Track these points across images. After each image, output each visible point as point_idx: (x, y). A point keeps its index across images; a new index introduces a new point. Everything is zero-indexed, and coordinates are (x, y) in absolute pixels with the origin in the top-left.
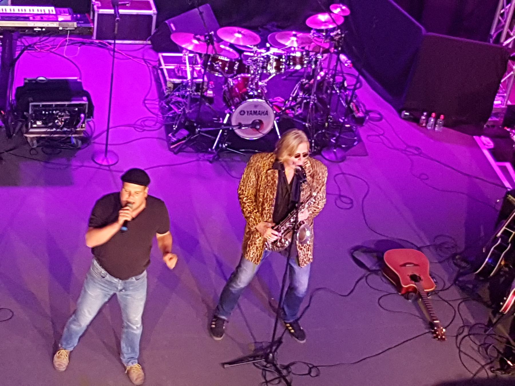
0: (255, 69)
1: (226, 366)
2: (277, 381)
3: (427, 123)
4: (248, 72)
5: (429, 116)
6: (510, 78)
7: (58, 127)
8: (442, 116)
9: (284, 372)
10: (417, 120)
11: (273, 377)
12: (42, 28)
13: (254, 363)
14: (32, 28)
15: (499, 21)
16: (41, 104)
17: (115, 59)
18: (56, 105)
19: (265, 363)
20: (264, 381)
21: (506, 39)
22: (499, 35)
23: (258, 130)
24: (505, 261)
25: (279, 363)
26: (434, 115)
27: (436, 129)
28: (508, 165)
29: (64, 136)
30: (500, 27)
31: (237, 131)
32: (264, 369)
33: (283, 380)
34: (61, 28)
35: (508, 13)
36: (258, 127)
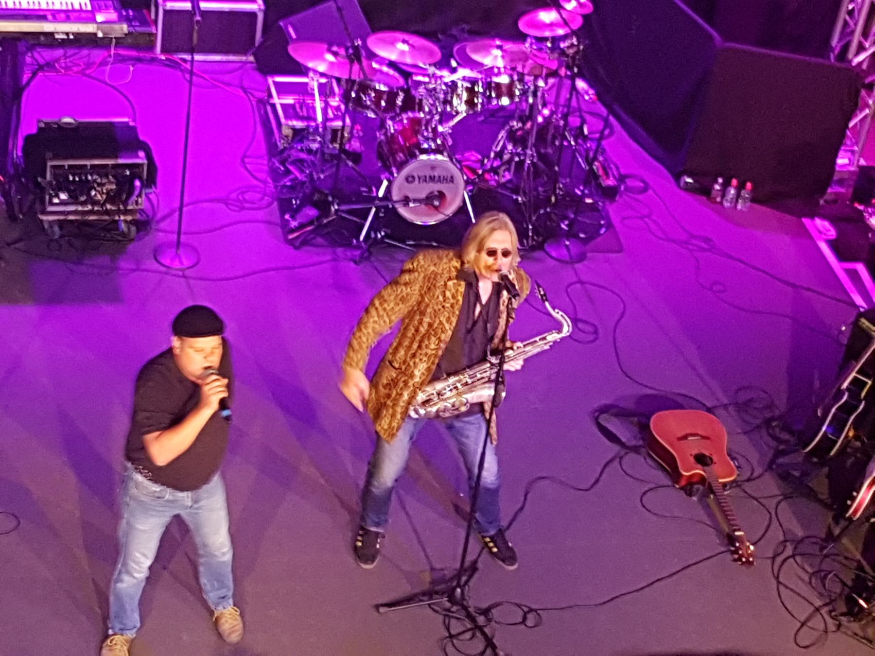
1: (382, 610)
2: (468, 635)
4: (421, 109)
5: (726, 185)
7: (94, 203)
9: (481, 620)
11: (461, 629)
12: (67, 34)
14: (52, 34)
15: (846, 23)
19: (448, 605)
22: (845, 48)
23: (436, 208)
24: (855, 429)
25: (472, 604)
26: (734, 182)
27: (739, 207)
28: (861, 268)
30: (848, 32)
31: (402, 211)
32: (447, 614)
35: (860, 11)
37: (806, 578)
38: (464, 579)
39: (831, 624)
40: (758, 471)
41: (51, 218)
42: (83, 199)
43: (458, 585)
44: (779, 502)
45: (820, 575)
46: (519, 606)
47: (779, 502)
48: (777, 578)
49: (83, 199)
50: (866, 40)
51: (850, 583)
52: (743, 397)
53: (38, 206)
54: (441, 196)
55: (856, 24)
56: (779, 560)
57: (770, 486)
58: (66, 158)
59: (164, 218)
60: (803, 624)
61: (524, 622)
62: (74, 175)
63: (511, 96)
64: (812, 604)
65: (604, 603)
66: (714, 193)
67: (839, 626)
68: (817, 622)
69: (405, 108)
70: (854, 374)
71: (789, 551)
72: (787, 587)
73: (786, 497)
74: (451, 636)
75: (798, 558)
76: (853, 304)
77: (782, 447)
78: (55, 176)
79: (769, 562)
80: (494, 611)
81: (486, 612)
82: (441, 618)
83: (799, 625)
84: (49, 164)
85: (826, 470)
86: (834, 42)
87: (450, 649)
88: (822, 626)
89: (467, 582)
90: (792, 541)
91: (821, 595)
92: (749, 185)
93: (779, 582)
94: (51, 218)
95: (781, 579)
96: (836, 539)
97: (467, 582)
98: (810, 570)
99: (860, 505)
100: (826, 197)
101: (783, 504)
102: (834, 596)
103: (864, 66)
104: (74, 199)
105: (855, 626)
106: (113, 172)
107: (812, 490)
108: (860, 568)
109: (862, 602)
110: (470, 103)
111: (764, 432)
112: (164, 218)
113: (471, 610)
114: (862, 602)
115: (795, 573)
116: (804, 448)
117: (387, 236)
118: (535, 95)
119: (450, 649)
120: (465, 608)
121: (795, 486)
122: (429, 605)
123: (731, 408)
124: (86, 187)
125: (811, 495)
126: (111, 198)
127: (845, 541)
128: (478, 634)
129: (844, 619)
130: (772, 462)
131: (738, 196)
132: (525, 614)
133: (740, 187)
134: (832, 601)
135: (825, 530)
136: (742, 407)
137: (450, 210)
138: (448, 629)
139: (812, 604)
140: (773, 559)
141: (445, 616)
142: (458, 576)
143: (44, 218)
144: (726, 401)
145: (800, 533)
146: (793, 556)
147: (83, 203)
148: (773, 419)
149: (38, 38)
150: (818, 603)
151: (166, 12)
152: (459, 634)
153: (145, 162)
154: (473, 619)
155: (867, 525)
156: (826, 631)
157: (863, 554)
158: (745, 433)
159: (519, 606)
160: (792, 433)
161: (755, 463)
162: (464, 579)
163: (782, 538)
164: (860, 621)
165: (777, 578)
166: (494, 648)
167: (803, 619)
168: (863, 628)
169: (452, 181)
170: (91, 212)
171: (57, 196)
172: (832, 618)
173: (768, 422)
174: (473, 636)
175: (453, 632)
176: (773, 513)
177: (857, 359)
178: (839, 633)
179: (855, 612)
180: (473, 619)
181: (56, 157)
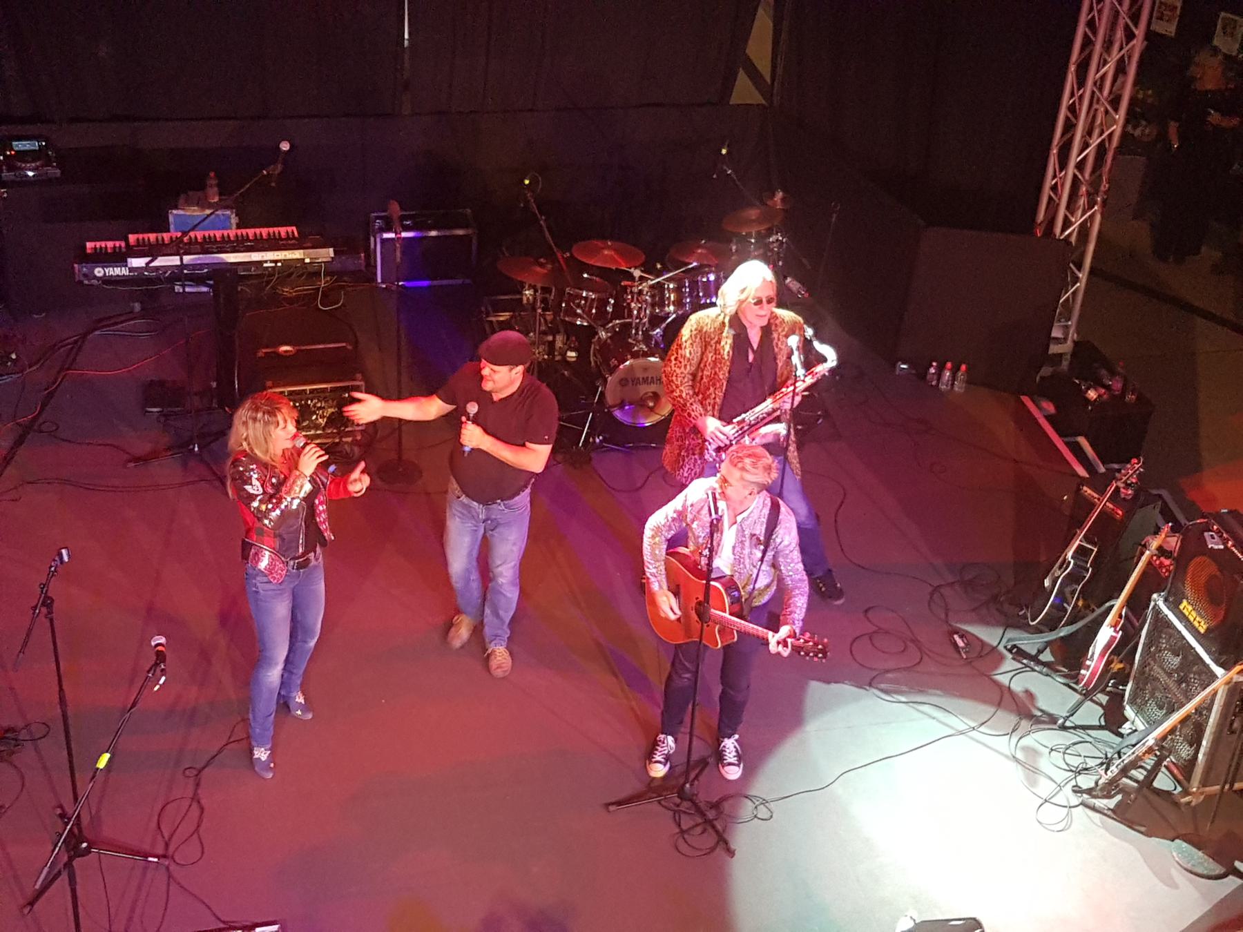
0: (640, 308)
1: (612, 808)
2: (699, 829)
3: (938, 380)
4: (630, 315)
5: (940, 369)
6: (1074, 293)
7: (317, 427)
8: (963, 367)
9: (711, 814)
10: (923, 375)
11: (692, 823)
12: (276, 262)
13: (659, 802)
14: (261, 263)
15: (1050, 198)
16: (308, 388)
17: (1041, 657)
18: (312, 391)
19: (678, 801)
20: (677, 830)
21: (1063, 230)
22: (1051, 222)
23: (652, 409)
24: (1085, 600)
25: (702, 798)
26: (949, 365)
27: (956, 389)
28: (1082, 441)
29: (329, 441)
30: (1053, 206)
31: (618, 414)
32: (677, 813)
33: (710, 830)
34: (307, 261)
35: (1063, 185)
36: (651, 404)
38: (692, 776)
50: (1072, 214)
58: (284, 386)
65: (25, 643)
70: (1078, 542)
74: (682, 832)
76: (1076, 475)
82: (671, 813)
86: (1041, 216)
89: (696, 777)
97: (696, 777)
103: (1073, 239)
113: (702, 805)
117: (604, 440)
119: (683, 847)
123: (957, 587)
141: (675, 812)
142: (687, 773)
152: (690, 829)
154: (703, 814)
158: (973, 610)
162: (692, 776)
174: (704, 831)
175: (684, 827)
177: (1080, 525)
180: (703, 814)
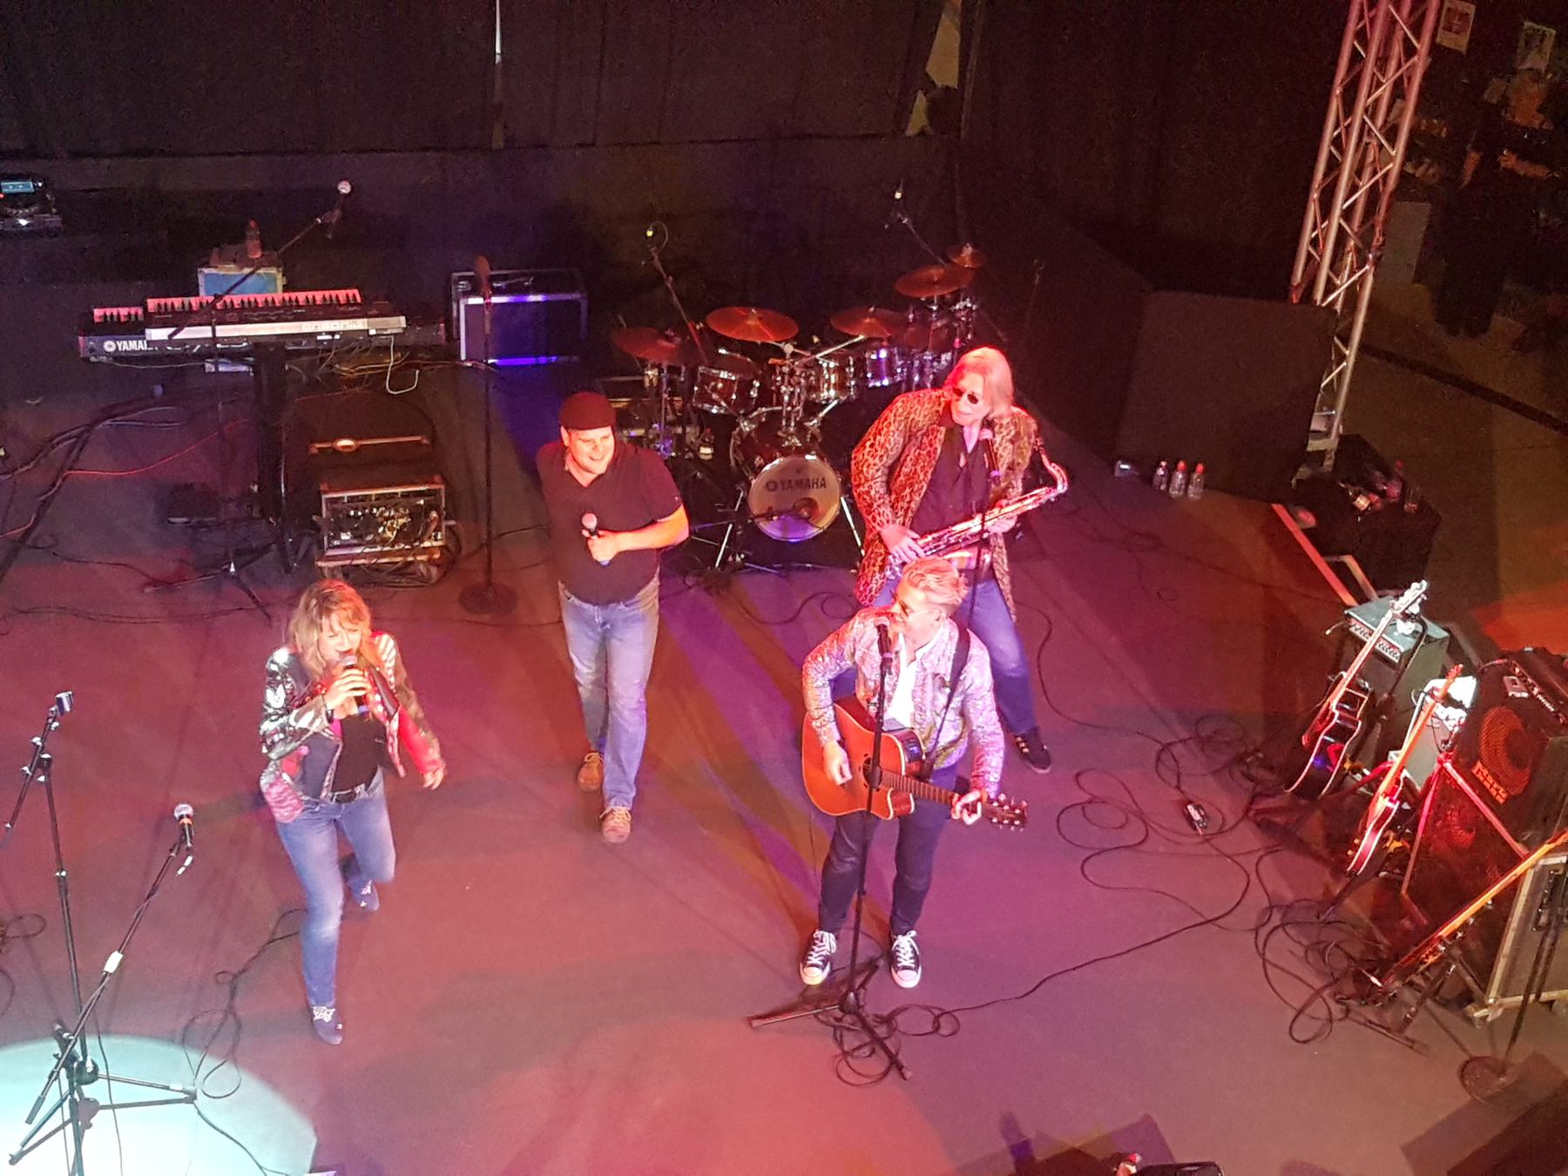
1: (756, 1023)
2: (867, 1051)
4: (780, 403)
5: (1170, 471)
7: (384, 542)
9: (881, 1031)
11: (857, 1044)
12: (332, 333)
14: (313, 335)
15: (1309, 256)
19: (839, 1014)
23: (807, 520)
24: (1353, 759)
25: (869, 1011)
30: (1312, 266)
32: (838, 1030)
35: (1325, 239)
37: (1300, 952)
38: (858, 981)
39: (1337, 1010)
40: (1230, 823)
41: (332, 564)
42: (369, 538)
43: (851, 989)
44: (1261, 858)
45: (1317, 949)
46: (928, 1008)
47: (1261, 858)
48: (1263, 955)
49: (369, 538)
51: (1357, 955)
52: (1206, 729)
53: (315, 551)
54: (811, 504)
55: (1321, 256)
56: (1263, 932)
57: (1248, 838)
59: (469, 556)
60: (1300, 1012)
61: (937, 1029)
62: (356, 509)
63: (892, 374)
64: (1465, 1050)
66: (1156, 481)
67: (1348, 1011)
68: (1318, 1008)
69: (761, 402)
71: (1276, 919)
72: (1275, 966)
73: (1270, 851)
74: (845, 1053)
75: (1291, 931)
77: (1259, 789)
78: (333, 511)
79: (1252, 936)
80: (899, 1018)
81: (888, 1020)
83: (1294, 1013)
84: (324, 497)
85: (1318, 813)
87: (846, 1073)
88: (1323, 1013)
89: (862, 985)
90: (1279, 907)
91: (1320, 973)
92: (1200, 467)
93: (1264, 961)
94: (332, 564)
95: (1268, 956)
96: (1337, 901)
98: (1305, 942)
99: (1363, 857)
100: (1298, 476)
101: (1266, 859)
102: (1336, 975)
103: (1338, 307)
104: (359, 537)
105: (1369, 1013)
106: (404, 501)
107: (1301, 841)
108: (1370, 937)
109: (1374, 980)
110: (841, 386)
111: (1237, 772)
112: (469, 556)
113: (870, 1020)
114: (1374, 980)
115: (1286, 948)
116: (1288, 787)
117: (747, 559)
118: (922, 372)
119: (846, 1073)
120: (862, 1020)
121: (1280, 835)
122: (815, 1015)
124: (370, 523)
125: (1301, 847)
126: (402, 535)
127: (1347, 901)
128: (878, 1049)
129: (1352, 1002)
130: (1248, 810)
131: (1188, 481)
132: (937, 1018)
133: (1189, 473)
134: (1336, 981)
135: (1321, 891)
136: (1204, 742)
137: (825, 523)
138: (841, 1044)
139: (1465, 1050)
140: (1256, 930)
141: (835, 1028)
143: (320, 564)
144: (1185, 735)
145: (1289, 896)
146: (1282, 925)
147: (373, 543)
148: (1247, 754)
149: (300, 344)
150: (1318, 984)
151: (467, 306)
153: (442, 487)
154: (871, 1032)
155: (1374, 880)
156: (1331, 1021)
157: (1374, 918)
159: (928, 1008)
160: (1271, 769)
161: (1224, 809)
163: (1266, 904)
164: (1375, 1002)
165: (1263, 955)
166: (900, 1068)
167: (1298, 1005)
168: (1378, 1014)
169: (824, 485)
170: (382, 554)
171: (338, 538)
172: (1338, 1002)
173: (1240, 759)
174: (873, 1052)
176: (1253, 877)
178: (1347, 1023)
179: (1367, 995)
180: (871, 1032)
181: (331, 490)
